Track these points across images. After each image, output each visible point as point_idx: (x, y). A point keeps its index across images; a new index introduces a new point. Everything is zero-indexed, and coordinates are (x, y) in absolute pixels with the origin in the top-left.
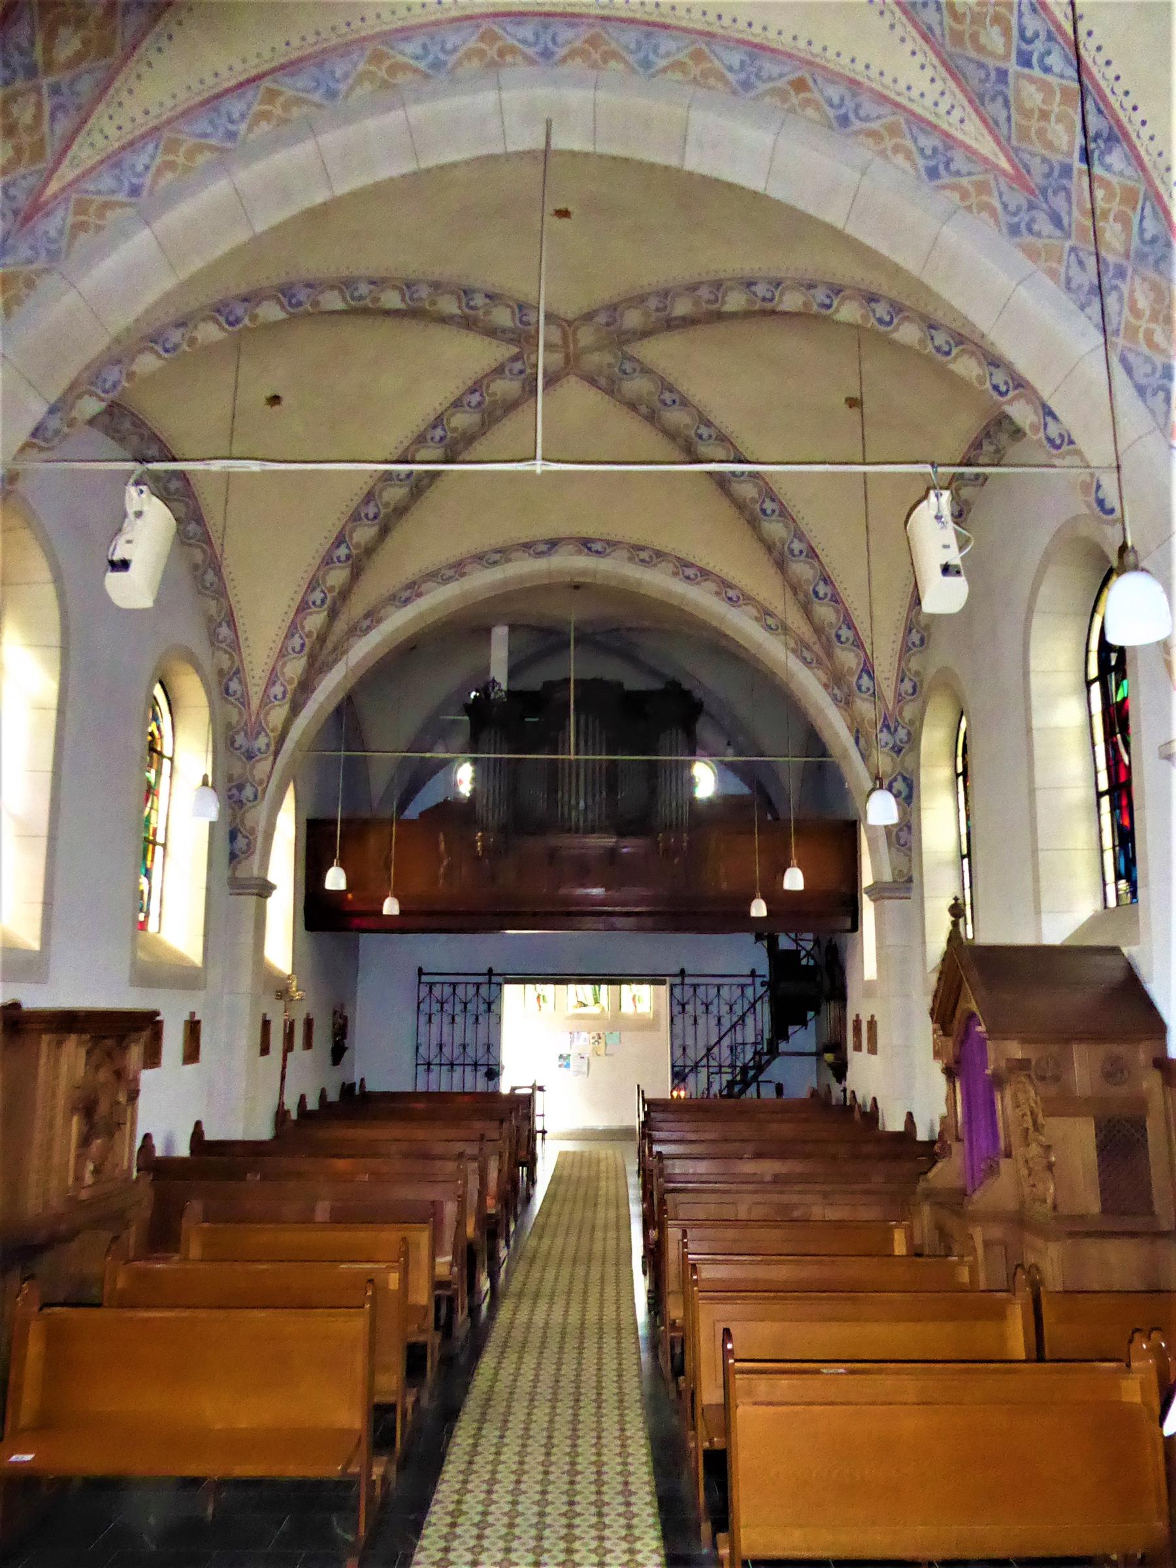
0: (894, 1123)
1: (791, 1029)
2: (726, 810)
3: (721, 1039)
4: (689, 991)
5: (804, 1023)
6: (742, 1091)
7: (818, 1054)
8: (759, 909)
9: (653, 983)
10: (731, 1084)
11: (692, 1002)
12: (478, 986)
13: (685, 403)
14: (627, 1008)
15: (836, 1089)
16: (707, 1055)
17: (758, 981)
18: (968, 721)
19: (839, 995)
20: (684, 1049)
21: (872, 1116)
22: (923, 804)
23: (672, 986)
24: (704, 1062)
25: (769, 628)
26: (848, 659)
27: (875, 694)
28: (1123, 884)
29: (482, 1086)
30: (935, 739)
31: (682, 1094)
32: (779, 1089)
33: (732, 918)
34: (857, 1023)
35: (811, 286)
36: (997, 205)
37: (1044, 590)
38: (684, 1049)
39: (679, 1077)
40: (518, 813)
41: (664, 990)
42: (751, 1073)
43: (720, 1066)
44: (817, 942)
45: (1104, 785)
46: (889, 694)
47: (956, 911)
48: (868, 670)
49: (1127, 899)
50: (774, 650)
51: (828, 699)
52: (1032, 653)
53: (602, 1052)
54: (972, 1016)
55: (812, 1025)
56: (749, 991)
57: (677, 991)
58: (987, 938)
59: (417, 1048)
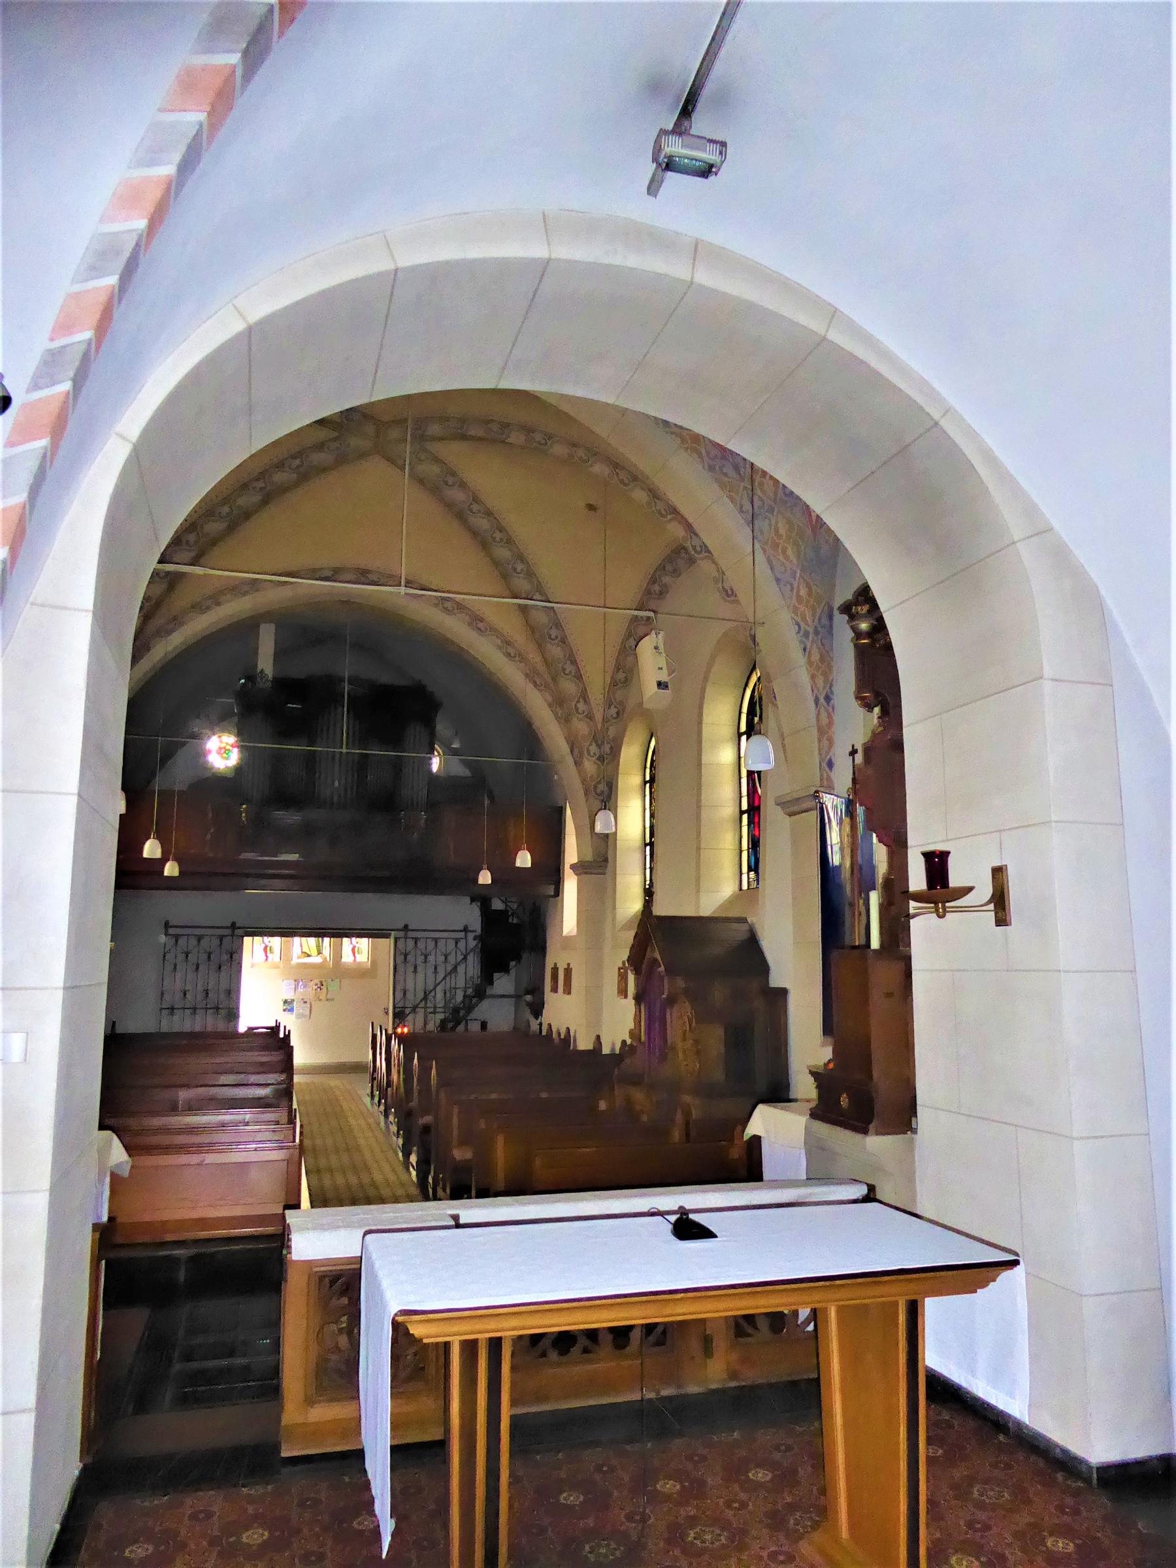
0: (584, 1043)
1: (496, 975)
2: (445, 791)
3: (436, 986)
4: (411, 943)
5: (506, 970)
6: (453, 1029)
7: (517, 997)
8: (485, 878)
9: (282, 935)
10: (443, 1022)
11: (433, 953)
12: (221, 938)
13: (463, 485)
14: (347, 957)
15: (534, 1025)
16: (425, 998)
17: (471, 936)
18: (657, 742)
19: (541, 948)
20: (405, 994)
21: (567, 1040)
23: (396, 940)
24: (422, 1004)
25: (508, 655)
26: (569, 687)
27: (590, 717)
28: (752, 874)
29: (221, 1026)
30: (631, 755)
31: (406, 1030)
32: (484, 1025)
33: (458, 882)
34: (555, 970)
35: (574, 445)
36: (704, 452)
37: (715, 669)
38: (405, 994)
39: (399, 1016)
40: (272, 789)
41: (386, 944)
42: (462, 1013)
43: (435, 1007)
44: (520, 904)
45: (745, 807)
46: (598, 716)
48: (584, 696)
49: (754, 885)
50: (512, 675)
51: (504, 659)
53: (323, 997)
54: (656, 960)
55: (513, 972)
56: (462, 944)
57: (401, 943)
59: (162, 994)
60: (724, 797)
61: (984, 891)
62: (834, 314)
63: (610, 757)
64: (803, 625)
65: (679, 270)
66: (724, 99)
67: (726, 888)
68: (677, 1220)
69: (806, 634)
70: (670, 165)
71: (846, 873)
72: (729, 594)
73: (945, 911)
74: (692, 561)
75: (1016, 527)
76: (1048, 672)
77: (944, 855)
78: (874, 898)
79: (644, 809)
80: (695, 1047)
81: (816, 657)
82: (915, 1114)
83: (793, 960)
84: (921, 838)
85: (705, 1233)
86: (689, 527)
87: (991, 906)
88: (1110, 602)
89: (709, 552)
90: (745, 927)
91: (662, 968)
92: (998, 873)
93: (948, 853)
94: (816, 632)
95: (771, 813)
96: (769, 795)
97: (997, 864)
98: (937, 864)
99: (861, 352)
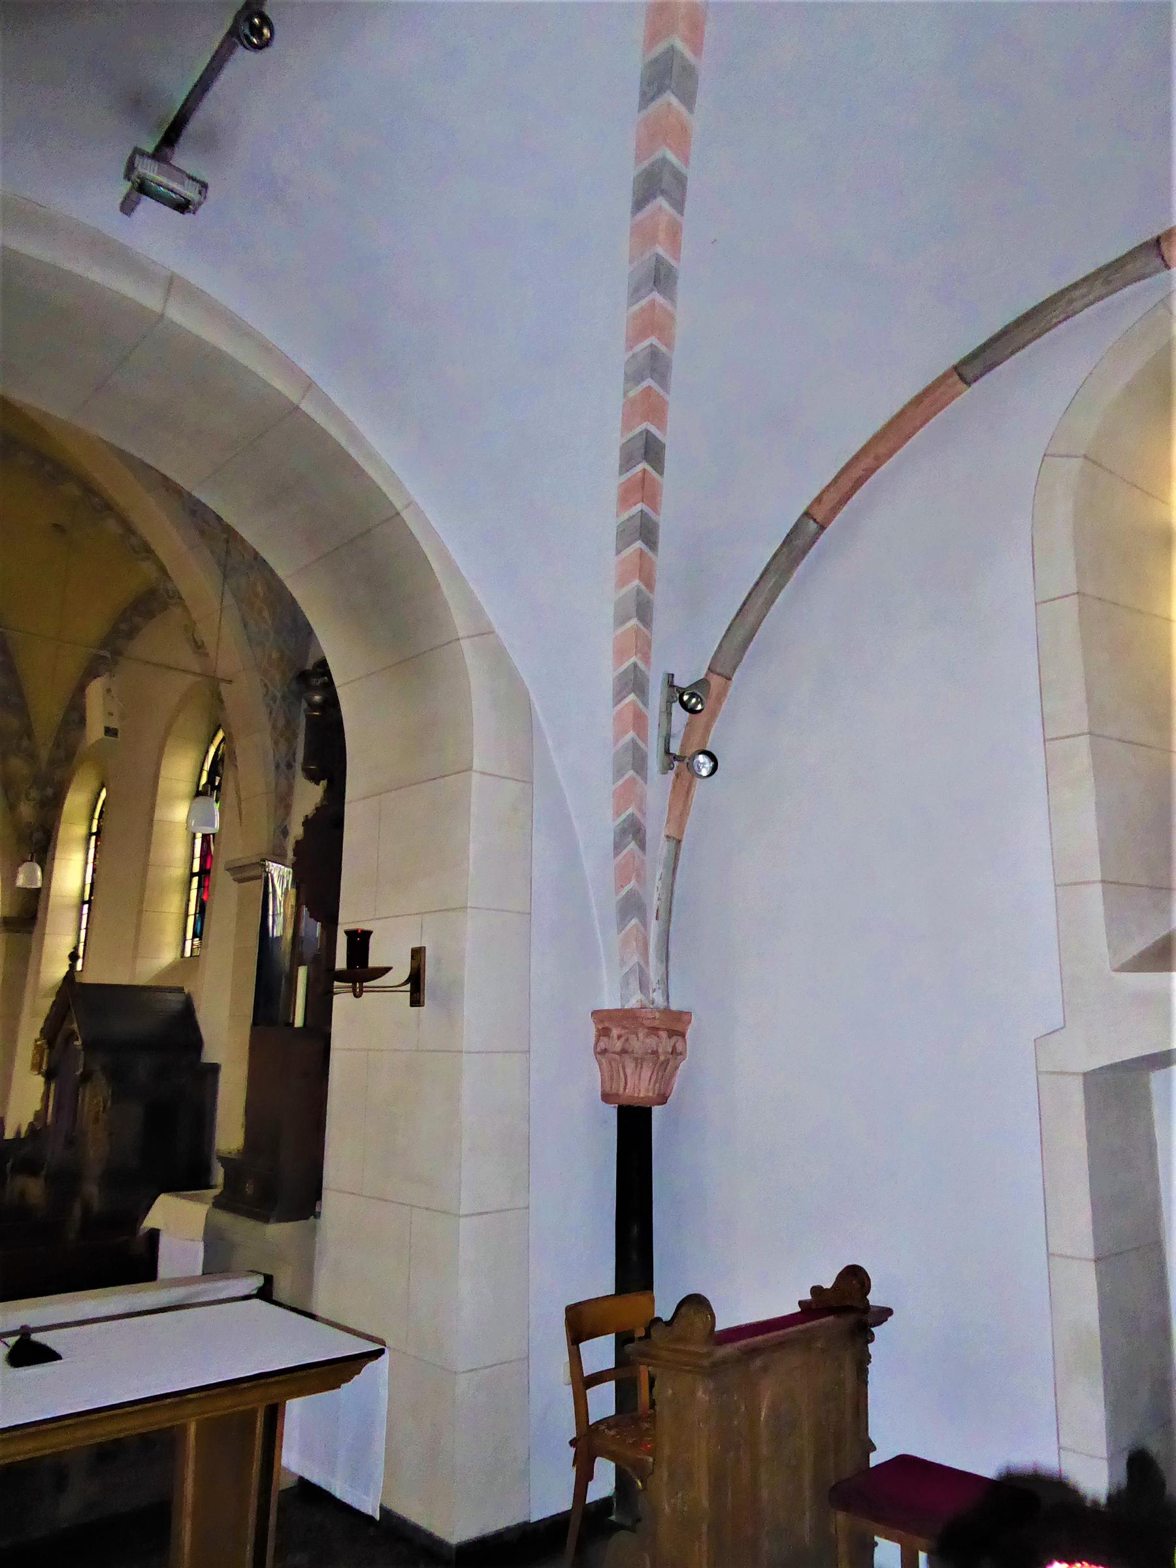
22: (57, 855)
27: (32, 757)
30: (76, 802)
45: (196, 869)
47: (74, 957)
52: (164, 763)
58: (89, 978)
60: (176, 854)
61: (401, 971)
62: (309, 386)
63: (52, 806)
64: (271, 688)
65: (151, 300)
66: (210, 143)
67: (168, 956)
68: (17, 1342)
69: (274, 699)
70: (143, 188)
71: (286, 946)
72: (198, 647)
73: (362, 991)
74: (165, 607)
75: (460, 622)
76: (476, 764)
77: (367, 934)
78: (302, 972)
79: (86, 863)
80: (105, 1128)
81: (281, 723)
82: (319, 1197)
83: (225, 1037)
84: (348, 919)
85: (47, 1355)
86: (163, 570)
87: (408, 987)
88: (537, 707)
89: (181, 598)
90: (180, 997)
91: (78, 1043)
92: (418, 954)
93: (370, 933)
94: (284, 698)
95: (221, 877)
96: (224, 856)
97: (417, 945)
98: (359, 941)
99: (333, 431)
